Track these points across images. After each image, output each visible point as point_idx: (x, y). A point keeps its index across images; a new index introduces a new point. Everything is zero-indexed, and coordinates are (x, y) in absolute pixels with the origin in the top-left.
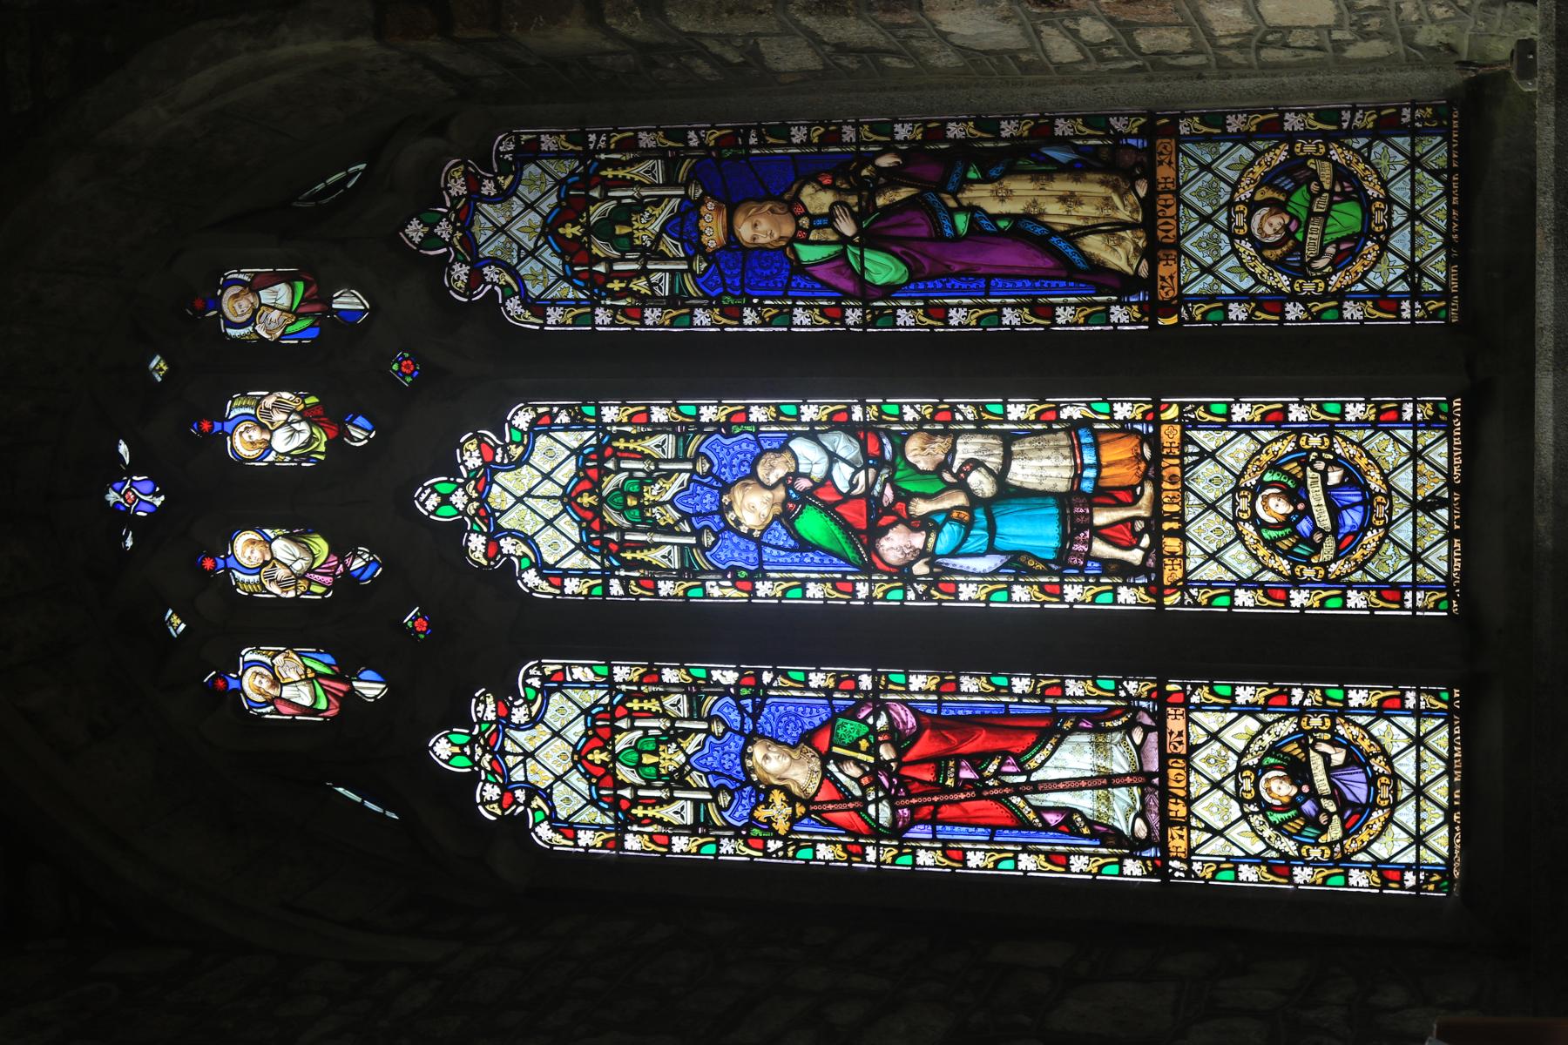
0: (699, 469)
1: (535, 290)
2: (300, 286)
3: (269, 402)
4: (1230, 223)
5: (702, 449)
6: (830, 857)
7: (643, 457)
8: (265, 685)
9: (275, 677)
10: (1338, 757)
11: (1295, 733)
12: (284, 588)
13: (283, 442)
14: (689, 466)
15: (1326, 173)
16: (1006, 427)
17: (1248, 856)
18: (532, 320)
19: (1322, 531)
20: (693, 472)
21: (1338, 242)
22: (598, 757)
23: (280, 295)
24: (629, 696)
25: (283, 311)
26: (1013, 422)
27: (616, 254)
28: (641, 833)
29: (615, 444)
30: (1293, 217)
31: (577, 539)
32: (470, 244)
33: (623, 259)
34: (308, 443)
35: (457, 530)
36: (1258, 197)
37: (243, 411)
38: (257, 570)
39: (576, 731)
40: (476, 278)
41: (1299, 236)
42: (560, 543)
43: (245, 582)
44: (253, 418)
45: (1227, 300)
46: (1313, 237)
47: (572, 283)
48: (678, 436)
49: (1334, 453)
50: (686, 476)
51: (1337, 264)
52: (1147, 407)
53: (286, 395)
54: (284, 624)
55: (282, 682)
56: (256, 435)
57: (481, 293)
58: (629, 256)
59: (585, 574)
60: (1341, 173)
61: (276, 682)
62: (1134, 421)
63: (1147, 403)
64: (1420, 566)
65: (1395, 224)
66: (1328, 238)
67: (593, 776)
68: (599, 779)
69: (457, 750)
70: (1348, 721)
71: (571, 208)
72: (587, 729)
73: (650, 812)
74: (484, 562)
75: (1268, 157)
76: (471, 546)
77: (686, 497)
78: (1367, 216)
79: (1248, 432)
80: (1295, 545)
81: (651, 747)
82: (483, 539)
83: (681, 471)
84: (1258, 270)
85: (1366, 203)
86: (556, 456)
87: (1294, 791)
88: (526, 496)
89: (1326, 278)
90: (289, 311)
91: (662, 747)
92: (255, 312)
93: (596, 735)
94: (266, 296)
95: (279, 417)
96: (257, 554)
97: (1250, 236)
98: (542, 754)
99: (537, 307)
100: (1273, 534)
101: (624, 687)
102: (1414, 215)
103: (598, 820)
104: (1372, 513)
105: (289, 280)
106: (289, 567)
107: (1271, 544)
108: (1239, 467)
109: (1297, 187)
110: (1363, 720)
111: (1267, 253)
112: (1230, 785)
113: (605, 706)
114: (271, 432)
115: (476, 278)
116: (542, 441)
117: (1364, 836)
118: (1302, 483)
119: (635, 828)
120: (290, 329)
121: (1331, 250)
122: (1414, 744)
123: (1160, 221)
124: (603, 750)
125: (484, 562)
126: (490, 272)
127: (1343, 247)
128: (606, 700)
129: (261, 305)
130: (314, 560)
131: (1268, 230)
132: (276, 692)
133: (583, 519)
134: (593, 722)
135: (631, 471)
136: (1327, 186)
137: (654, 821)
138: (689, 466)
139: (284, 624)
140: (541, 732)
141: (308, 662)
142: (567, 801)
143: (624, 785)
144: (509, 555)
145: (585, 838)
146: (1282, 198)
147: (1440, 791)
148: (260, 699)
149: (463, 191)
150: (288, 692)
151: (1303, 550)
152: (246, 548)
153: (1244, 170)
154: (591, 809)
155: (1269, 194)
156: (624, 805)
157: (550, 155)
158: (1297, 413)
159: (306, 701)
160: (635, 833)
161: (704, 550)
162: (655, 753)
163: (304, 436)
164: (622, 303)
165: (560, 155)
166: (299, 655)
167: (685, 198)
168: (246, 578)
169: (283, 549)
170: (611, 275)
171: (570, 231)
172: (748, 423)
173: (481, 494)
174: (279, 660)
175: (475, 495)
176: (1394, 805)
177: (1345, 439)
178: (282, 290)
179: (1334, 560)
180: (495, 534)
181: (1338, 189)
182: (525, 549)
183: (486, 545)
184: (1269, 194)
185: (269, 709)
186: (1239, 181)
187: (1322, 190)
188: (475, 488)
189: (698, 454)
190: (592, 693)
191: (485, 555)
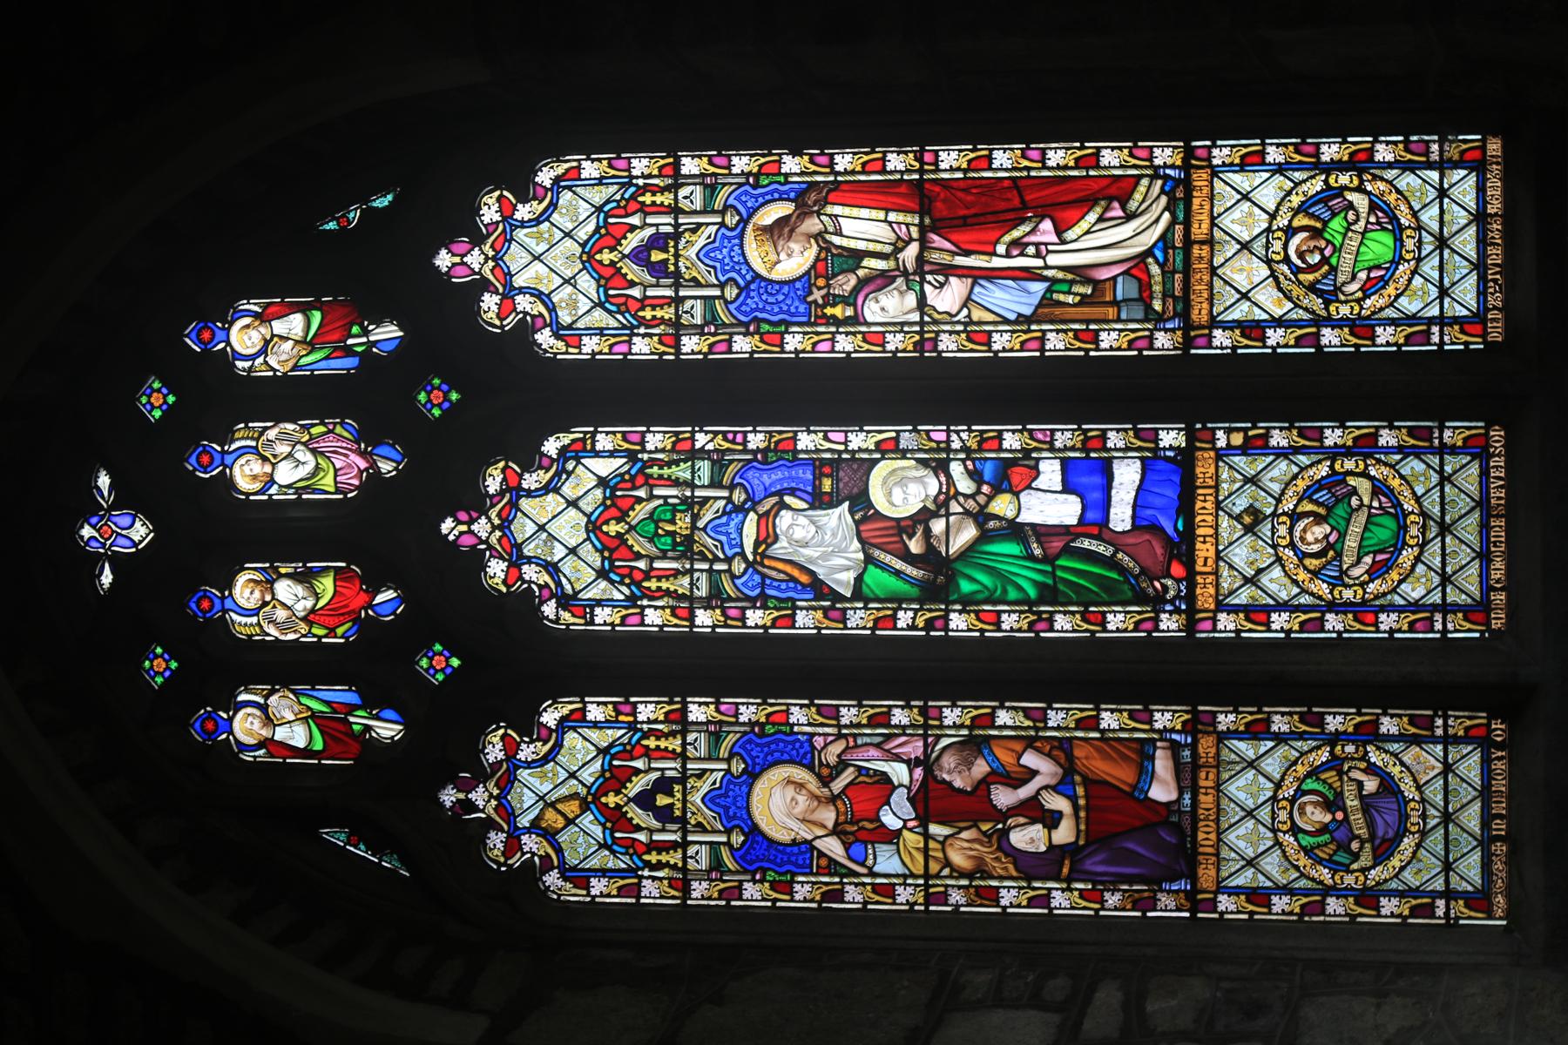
0: (734, 770)
1: (572, 860)
2: (317, 317)
3: (272, 434)
4: (1273, 819)
5: (731, 201)
6: (849, 348)
7: (676, 483)
8: (257, 725)
9: (268, 717)
10: (1371, 785)
11: (1323, 191)
12: (283, 631)
13: (286, 474)
14: (725, 493)
15: (1364, 486)
16: (1046, 173)
17: (1278, 887)
18: (574, 891)
19: (1358, 837)
20: (722, 224)
21: (1370, 269)
22: (613, 528)
23: (293, 325)
24: (646, 735)
25: (297, 342)
26: (1053, 728)
27: (658, 825)
28: (650, 335)
29: (645, 742)
30: (1333, 528)
31: (594, 296)
32: (509, 814)
33: (663, 830)
34: (314, 474)
35: (476, 559)
36: (1296, 223)
37: (243, 443)
38: (255, 612)
39: (590, 503)
40: (513, 845)
41: (1334, 261)
42: (579, 301)
43: (242, 624)
44: (255, 450)
45: (1267, 610)
46: (1348, 258)
47: (613, 852)
48: (706, 186)
49: (1368, 761)
50: (722, 503)
51: (1376, 571)
52: (1187, 717)
53: (290, 427)
54: (286, 666)
55: (275, 723)
56: (257, 467)
57: (510, 321)
58: (669, 826)
59: (601, 332)
60: (1379, 489)
61: (269, 721)
62: (1173, 730)
63: (1186, 712)
64: (1446, 200)
65: (1424, 253)
66: (1360, 266)
67: (601, 277)
68: (607, 280)
69: (457, 259)
70: (1379, 461)
71: (608, 235)
72: (605, 498)
73: (664, 585)
74: (504, 590)
75: (1304, 187)
76: (484, 306)
77: (713, 250)
78: (1399, 241)
79: (1286, 456)
80: (1335, 852)
81: (669, 516)
82: (504, 565)
83: (708, 224)
84: (1301, 864)
85: (1398, 231)
86: (577, 212)
87: (1328, 818)
88: (551, 525)
89: (1363, 585)
90: (303, 342)
91: (679, 515)
92: (267, 342)
93: (614, 505)
94: (279, 327)
95: (283, 449)
96: (257, 594)
97: (1292, 545)
98: (553, 783)
99: (579, 877)
100: (1312, 840)
101: (645, 727)
102: (1442, 242)
103: (610, 865)
104: (1406, 532)
105: (304, 309)
106: (289, 608)
107: (1308, 851)
108: (1271, 207)
109: (1334, 215)
110: (1395, 747)
111: (1307, 562)
112: (1258, 247)
113: (624, 745)
114: (274, 465)
115: (513, 845)
116: (566, 196)
117: (1396, 862)
118: (1340, 795)
119: (642, 330)
120: (304, 361)
121: (1363, 275)
122: (1444, 775)
123: (1198, 518)
124: (618, 793)
125: (504, 590)
126: (523, 302)
127: (1380, 557)
128: (625, 740)
129: (273, 336)
130: (318, 599)
131: (1309, 537)
132: (266, 733)
133: (605, 548)
134: (605, 220)
135: (665, 498)
136: (1366, 501)
137: (668, 593)
138: (725, 493)
139: (286, 666)
140: (553, 502)
141: (304, 700)
142: (581, 573)
143: (638, 828)
144: (531, 582)
145: (590, 344)
146: (1319, 225)
147: (1471, 818)
148: (253, 741)
149: (497, 217)
150: (281, 734)
151: (1342, 858)
152: (244, 591)
153: (1287, 485)
154: (598, 313)
155: (1306, 222)
156: (633, 306)
157: (595, 725)
158: (1332, 437)
159: (300, 742)
160: (644, 336)
161: (733, 577)
162: (672, 521)
163: (312, 464)
164: (656, 331)
165: (600, 181)
166: (294, 692)
167: (728, 771)
168: (244, 620)
169: (286, 590)
170: (647, 575)
171: (606, 257)
172: (780, 174)
173: (497, 253)
174: (273, 700)
175: (491, 253)
176: (1424, 834)
177: (1379, 461)
178: (297, 320)
179: (1373, 867)
180: (509, 293)
181: (1376, 504)
182: (547, 578)
183: (500, 306)
184: (1306, 222)
185: (262, 752)
186: (1283, 493)
187: (1362, 505)
188: (499, 515)
189: (726, 207)
190: (610, 732)
191: (498, 316)
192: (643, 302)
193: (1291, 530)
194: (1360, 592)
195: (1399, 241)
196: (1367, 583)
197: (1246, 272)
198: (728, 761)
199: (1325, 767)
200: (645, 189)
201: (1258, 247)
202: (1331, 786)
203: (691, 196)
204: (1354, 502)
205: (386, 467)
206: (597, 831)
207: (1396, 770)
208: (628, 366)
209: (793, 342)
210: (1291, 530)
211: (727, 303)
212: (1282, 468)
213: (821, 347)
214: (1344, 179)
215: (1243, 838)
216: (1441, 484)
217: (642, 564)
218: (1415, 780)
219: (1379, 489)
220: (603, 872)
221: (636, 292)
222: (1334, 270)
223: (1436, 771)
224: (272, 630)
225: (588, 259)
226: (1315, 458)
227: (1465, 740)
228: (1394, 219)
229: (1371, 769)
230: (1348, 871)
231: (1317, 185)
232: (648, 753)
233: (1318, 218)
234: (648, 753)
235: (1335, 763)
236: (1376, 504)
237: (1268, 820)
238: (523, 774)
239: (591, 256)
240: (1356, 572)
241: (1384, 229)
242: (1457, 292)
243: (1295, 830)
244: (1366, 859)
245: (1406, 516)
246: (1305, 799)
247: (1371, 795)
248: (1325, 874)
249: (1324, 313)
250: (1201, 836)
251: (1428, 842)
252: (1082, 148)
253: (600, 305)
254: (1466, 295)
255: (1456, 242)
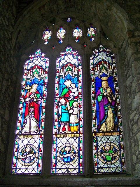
10: (72, 157)
15: (115, 155)
21: (105, 157)
24: (77, 68)
30: (109, 151)
33: (99, 68)
40: (96, 53)
42: (63, 62)
51: (102, 157)
60: (115, 157)
71: (106, 62)
75: (117, 147)
78: (110, 161)
84: (101, 146)
86: (75, 61)
89: (100, 156)
98: (38, 61)
99: (93, 59)
102: (109, 168)
111: (104, 147)
115: (96, 53)
118: (71, 153)
119: (94, 67)
122: (33, 168)
131: (107, 148)
136: (113, 155)
151: (61, 153)
155: (112, 148)
162: (37, 74)
170: (31, 72)
180: (65, 55)
184: (112, 148)
192: (31, 72)
193: (29, 147)
194: (99, 155)
195: (110, 161)
196: (101, 156)
197: (26, 142)
198: (109, 75)
199: (75, 151)
200: (44, 70)
201: (29, 143)
202: (72, 151)
203: (43, 76)
204: (113, 154)
205: (46, 43)
206: (99, 61)
207: (74, 161)
208: (55, 67)
209: (57, 85)
210: (29, 147)
211: (62, 78)
212: (37, 146)
213: (57, 88)
214: (37, 155)
215: (64, 140)
216: (116, 167)
217: (64, 68)
218: (115, 163)
219: (115, 157)
220: (28, 67)
221: (98, 66)
222: (105, 152)
223: (101, 166)
224: (58, 33)
225: (69, 63)
226: (78, 149)
227: (79, 170)
228: (113, 160)
229: (74, 158)
230: (20, 155)
231: (118, 149)
232: (41, 71)
233: (113, 149)
234: (41, 71)
235: (35, 153)
236: (113, 157)
237: (28, 144)
238: (105, 53)
239: (36, 65)
240: (102, 155)
241: (112, 159)
242: (20, 170)
243: (65, 147)
244: (22, 157)
245: (111, 161)
246: (70, 148)
247: (70, 157)
248: (100, 150)
249: (98, 151)
250: (29, 136)
251: (64, 166)
252: (82, 119)
253: (97, 62)
254: (19, 172)
255: (27, 171)
